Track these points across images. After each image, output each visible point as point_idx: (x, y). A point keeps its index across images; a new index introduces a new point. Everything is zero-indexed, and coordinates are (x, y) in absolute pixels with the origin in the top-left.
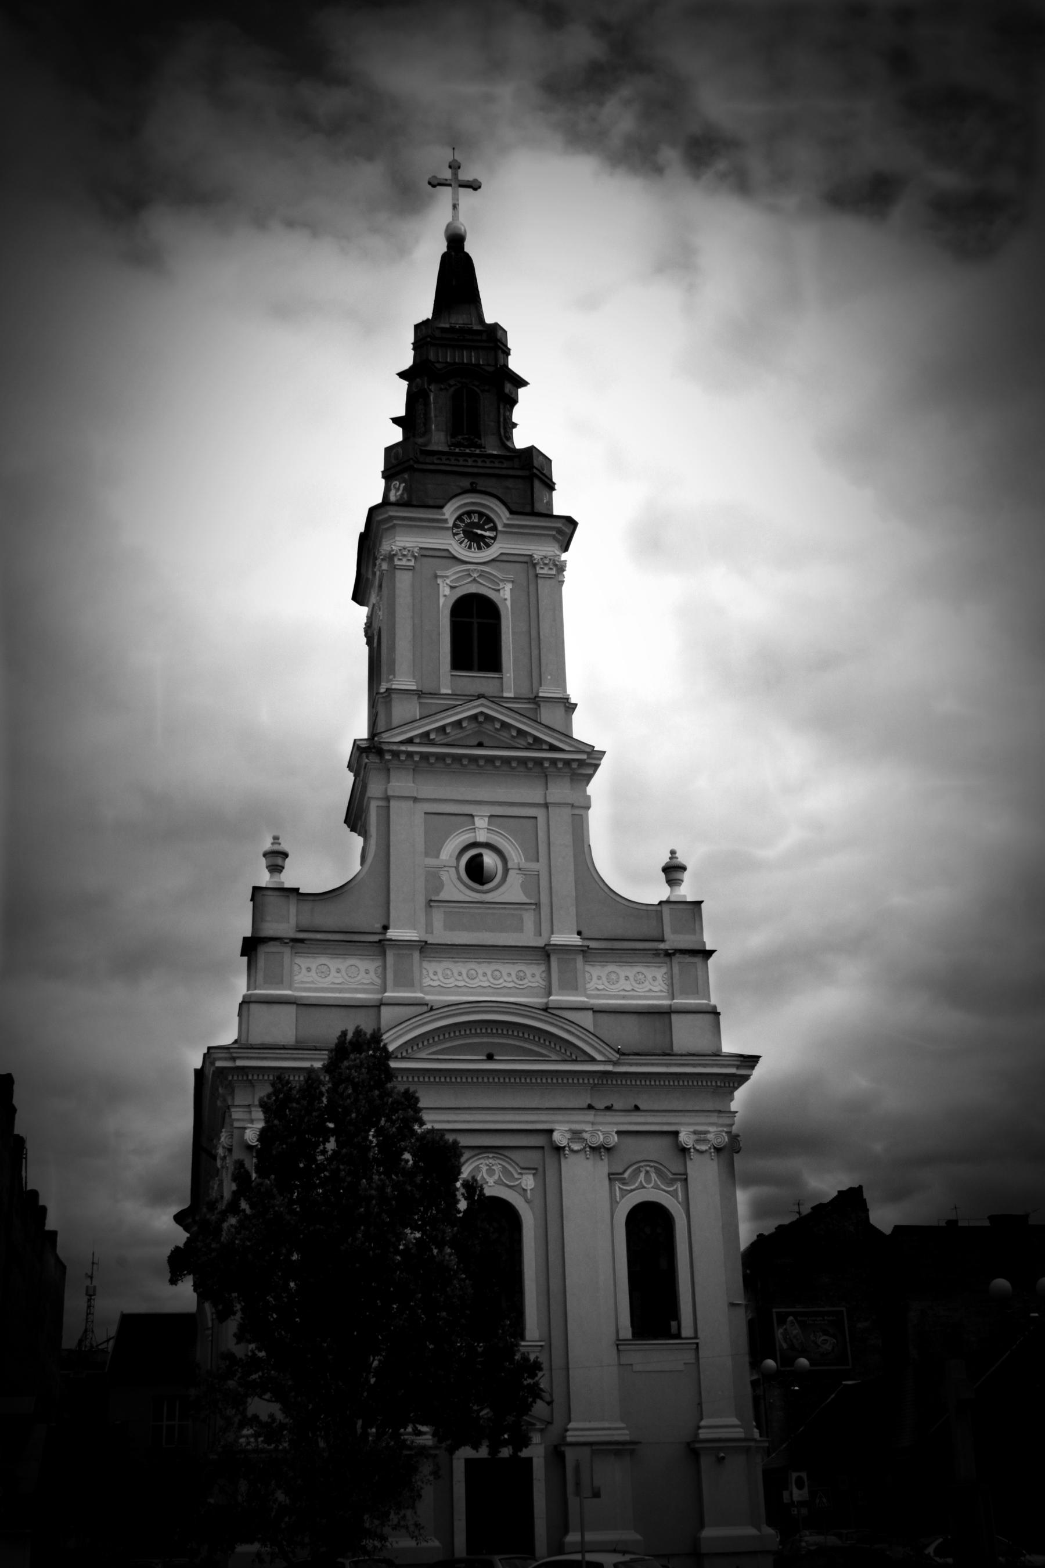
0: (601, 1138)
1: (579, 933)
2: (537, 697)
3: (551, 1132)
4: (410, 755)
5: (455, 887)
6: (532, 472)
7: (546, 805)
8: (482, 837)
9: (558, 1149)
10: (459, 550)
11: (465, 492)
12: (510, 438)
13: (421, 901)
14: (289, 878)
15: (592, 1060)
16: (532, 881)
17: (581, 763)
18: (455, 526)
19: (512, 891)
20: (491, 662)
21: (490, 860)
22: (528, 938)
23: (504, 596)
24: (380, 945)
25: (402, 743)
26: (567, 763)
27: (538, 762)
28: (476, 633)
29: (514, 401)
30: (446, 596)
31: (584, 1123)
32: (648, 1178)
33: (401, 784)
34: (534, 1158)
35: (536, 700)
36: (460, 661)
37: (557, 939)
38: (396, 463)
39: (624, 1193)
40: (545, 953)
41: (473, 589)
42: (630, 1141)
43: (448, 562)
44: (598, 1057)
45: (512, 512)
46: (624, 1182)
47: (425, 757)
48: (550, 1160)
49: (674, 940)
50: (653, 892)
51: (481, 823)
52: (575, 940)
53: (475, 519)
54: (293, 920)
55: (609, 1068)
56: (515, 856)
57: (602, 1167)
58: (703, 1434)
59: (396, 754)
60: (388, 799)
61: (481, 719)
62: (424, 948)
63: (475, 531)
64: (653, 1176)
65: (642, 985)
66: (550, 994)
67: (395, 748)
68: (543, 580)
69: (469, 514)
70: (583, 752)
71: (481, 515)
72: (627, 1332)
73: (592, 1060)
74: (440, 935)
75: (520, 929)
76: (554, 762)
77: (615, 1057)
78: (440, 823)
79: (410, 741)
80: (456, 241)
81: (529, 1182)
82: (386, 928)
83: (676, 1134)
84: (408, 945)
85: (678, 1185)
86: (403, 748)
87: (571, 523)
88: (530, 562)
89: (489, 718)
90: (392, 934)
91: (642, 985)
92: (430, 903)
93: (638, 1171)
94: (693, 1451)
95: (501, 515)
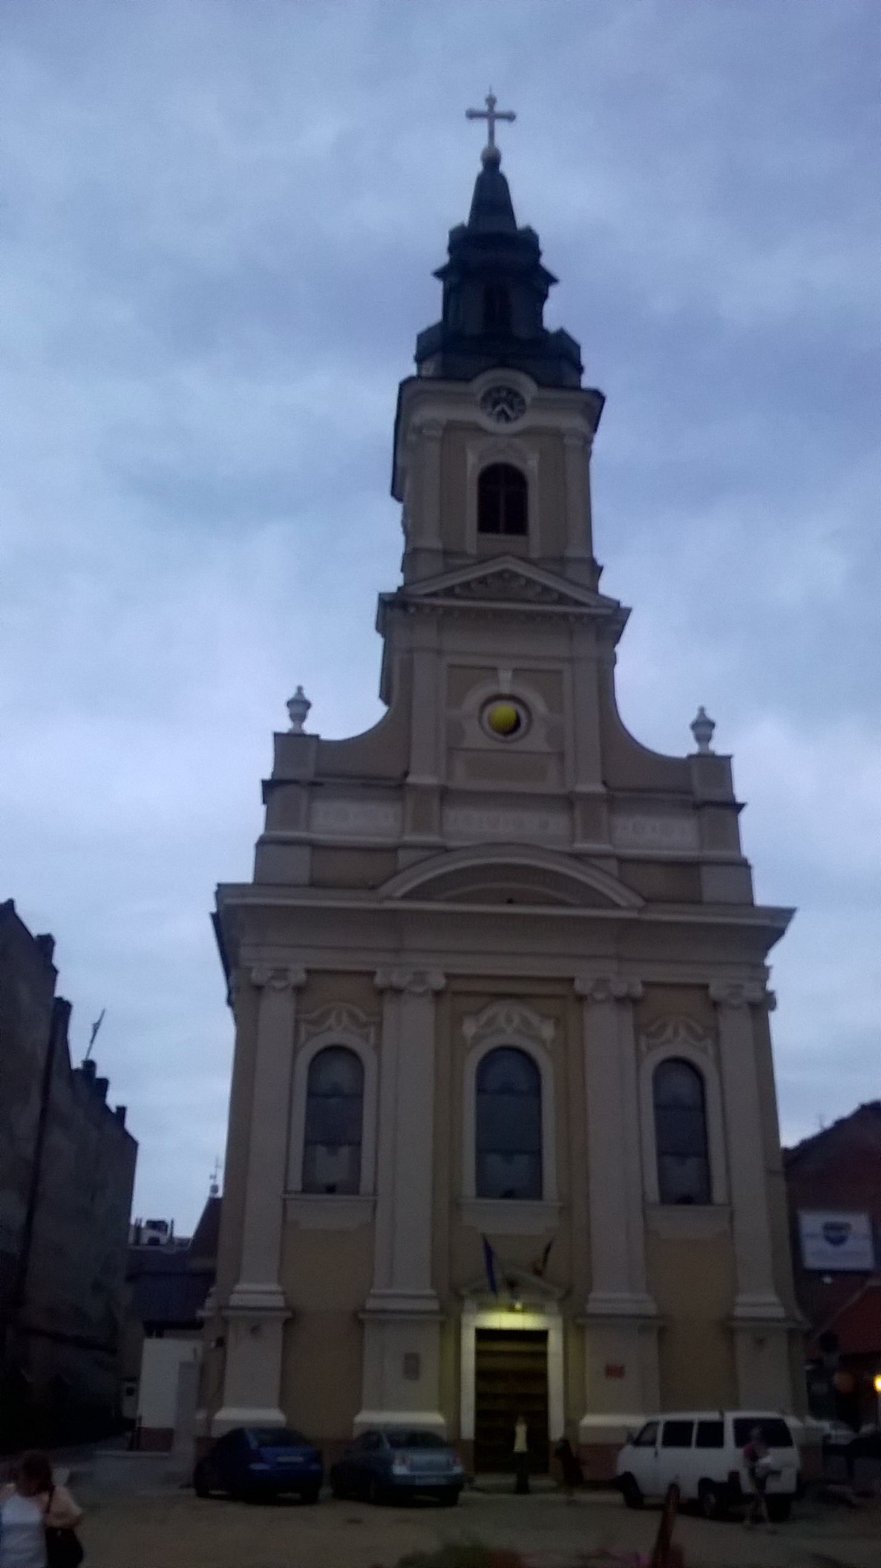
0: (621, 989)
1: (605, 783)
2: (731, 1318)
3: (572, 980)
4: (434, 608)
5: (476, 737)
6: (559, 359)
7: (571, 660)
8: (505, 689)
9: (581, 999)
10: (486, 421)
11: (494, 367)
12: (539, 316)
14: (310, 727)
15: (616, 906)
17: (608, 619)
19: (535, 740)
20: (517, 524)
22: (550, 785)
23: (531, 465)
24: (396, 787)
25: (428, 595)
26: (593, 618)
27: (565, 616)
28: (503, 499)
29: (545, 296)
30: (473, 463)
32: (676, 1032)
35: (562, 560)
36: (487, 523)
37: (582, 788)
38: (428, 347)
39: (650, 1048)
40: (568, 802)
41: (500, 459)
44: (623, 903)
45: (540, 384)
47: (448, 611)
49: (702, 792)
50: (678, 744)
51: (505, 676)
52: (598, 788)
53: (504, 394)
56: (539, 706)
57: (628, 1018)
58: (739, 1312)
59: (419, 607)
60: (410, 651)
61: (506, 575)
62: (445, 795)
63: (504, 402)
65: (671, 835)
66: (573, 842)
67: (418, 600)
68: (572, 455)
69: (498, 390)
70: (609, 607)
71: (510, 391)
72: (654, 1195)
73: (616, 906)
74: (461, 780)
76: (579, 617)
77: (640, 903)
79: (434, 595)
80: (492, 161)
81: (548, 1031)
82: (406, 774)
83: (705, 987)
84: (426, 790)
85: (709, 1043)
86: (427, 601)
87: (598, 398)
88: (557, 434)
89: (515, 576)
90: (411, 779)
91: (671, 835)
92: (451, 750)
94: (728, 1328)
95: (528, 388)
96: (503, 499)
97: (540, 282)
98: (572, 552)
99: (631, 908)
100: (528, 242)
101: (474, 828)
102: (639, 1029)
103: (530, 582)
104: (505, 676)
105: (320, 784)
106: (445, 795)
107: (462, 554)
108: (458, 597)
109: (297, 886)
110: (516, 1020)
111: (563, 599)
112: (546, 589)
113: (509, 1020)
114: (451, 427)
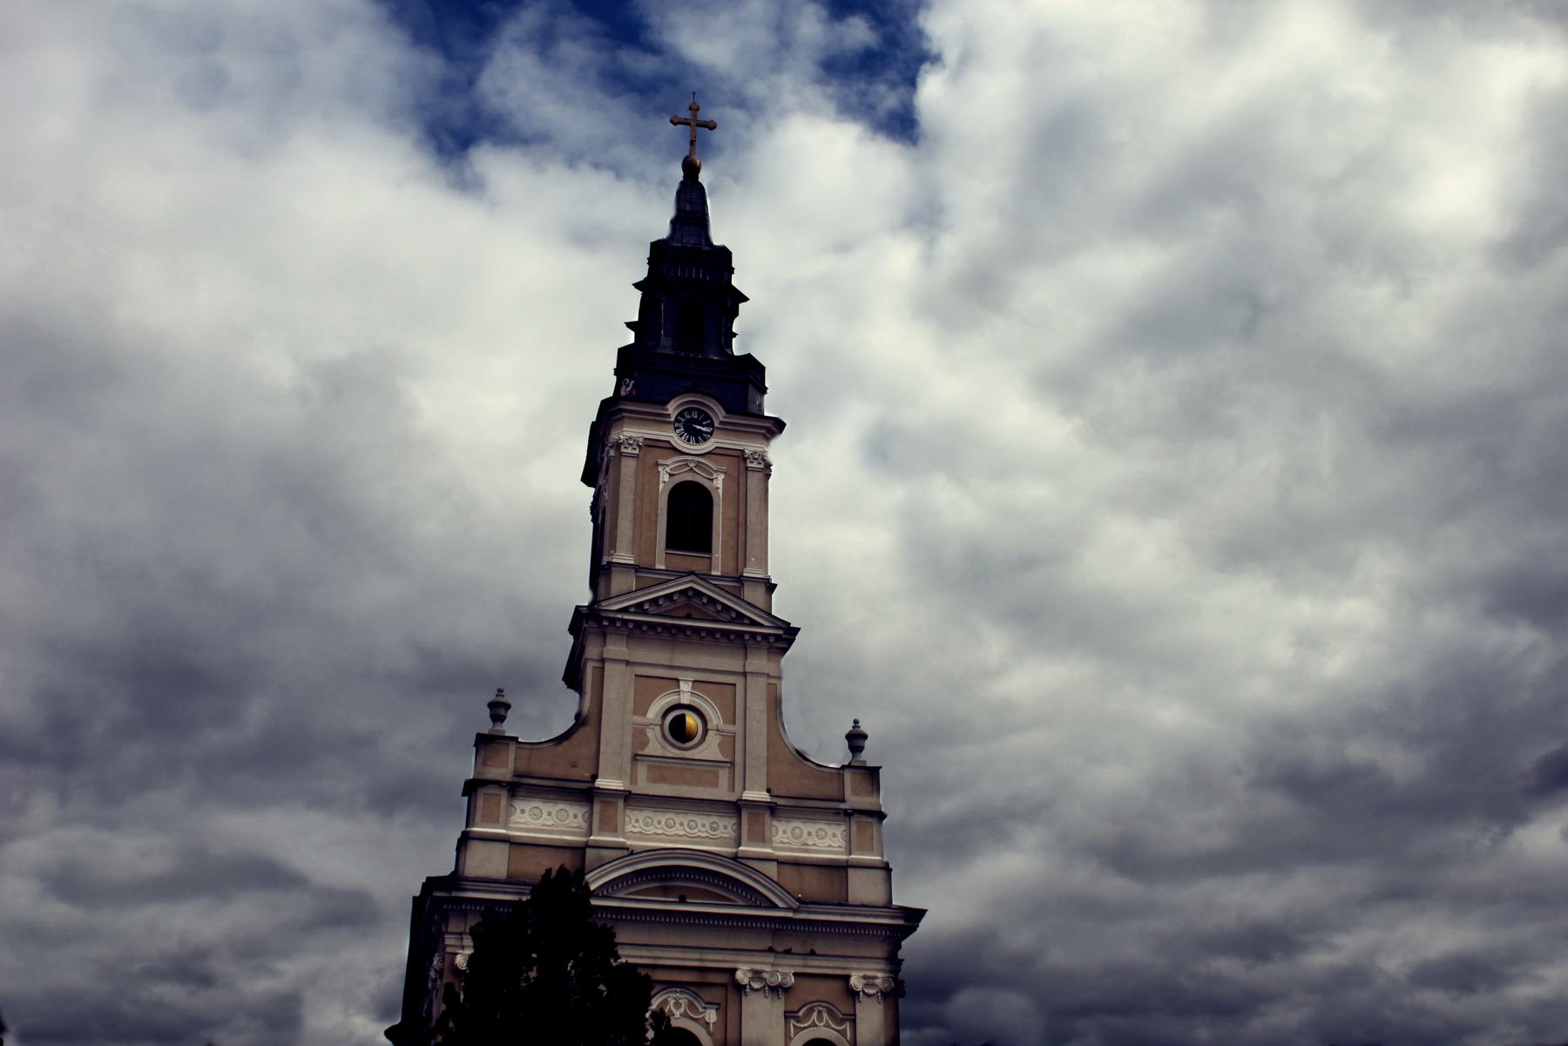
1: (768, 791)
5: (656, 745)
7: (745, 674)
13: (628, 755)
15: (774, 907)
16: (729, 741)
18: (677, 420)
19: (710, 749)
20: (703, 544)
21: (691, 720)
22: (721, 792)
23: (718, 484)
25: (619, 611)
26: (766, 636)
27: (740, 634)
28: (690, 515)
31: (765, 964)
33: (616, 648)
34: (717, 995)
35: (740, 580)
36: (673, 542)
37: (749, 795)
39: (798, 1030)
40: (736, 808)
41: (689, 477)
42: (806, 983)
43: (671, 452)
44: (781, 904)
45: (729, 411)
46: (798, 1020)
47: (638, 624)
48: (732, 996)
51: (685, 687)
52: (762, 796)
54: (511, 765)
55: (790, 915)
56: (715, 718)
57: (778, 1007)
59: (613, 621)
60: (603, 661)
62: (629, 798)
63: (693, 427)
64: (825, 1016)
68: (752, 474)
69: (690, 410)
71: (700, 412)
73: (774, 907)
74: (644, 786)
75: (715, 784)
76: (754, 635)
77: (796, 904)
78: (649, 685)
79: (625, 610)
81: (711, 1016)
82: (595, 777)
83: (848, 977)
85: (848, 1025)
88: (741, 456)
89: (699, 594)
90: (601, 783)
93: (811, 1011)
95: (719, 414)
96: (690, 515)
97: (623, 353)
98: (748, 572)
99: (789, 909)
100: (722, 259)
101: (650, 832)
102: (788, 1015)
103: (712, 601)
104: (685, 687)
105: (520, 785)
106: (629, 798)
107: (652, 570)
108: (645, 613)
109: (496, 881)
110: (683, 1002)
111: (740, 618)
112: (726, 608)
113: (677, 1005)
114: (651, 444)
